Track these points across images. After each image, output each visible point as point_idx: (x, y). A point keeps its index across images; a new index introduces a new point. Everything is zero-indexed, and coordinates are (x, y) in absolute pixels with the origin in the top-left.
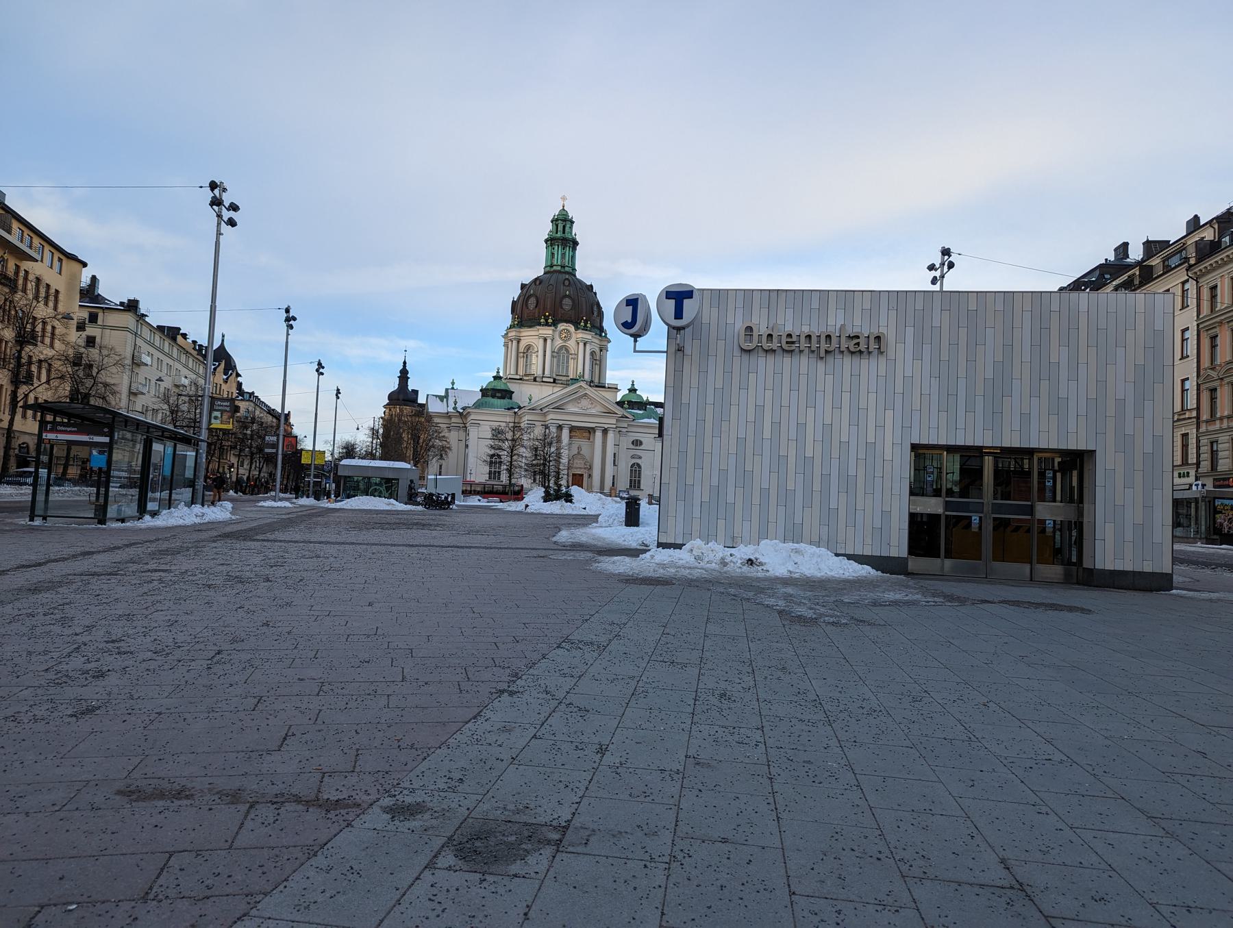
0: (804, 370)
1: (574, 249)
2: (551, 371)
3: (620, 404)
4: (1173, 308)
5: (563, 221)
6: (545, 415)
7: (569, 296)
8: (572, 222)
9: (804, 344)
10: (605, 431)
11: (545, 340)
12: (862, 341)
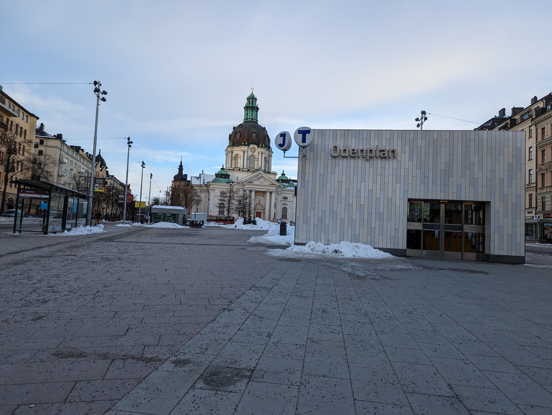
0: (360, 165)
1: (257, 111)
2: (247, 166)
3: (278, 181)
5: (252, 99)
6: (244, 185)
7: (255, 133)
8: (256, 99)
9: (360, 154)
10: (271, 193)
11: (244, 152)
12: (386, 152)
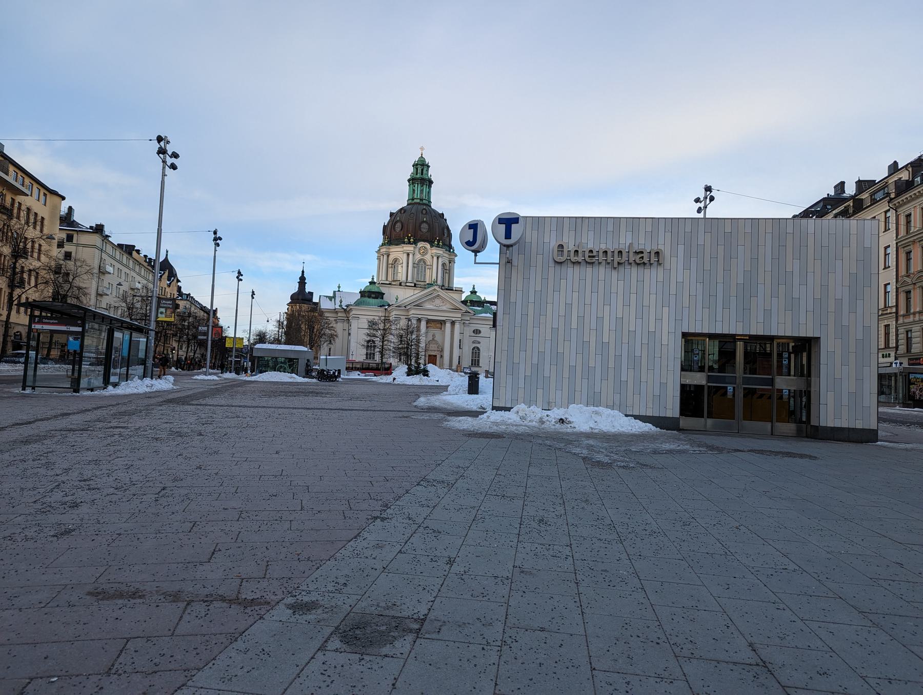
0: (602, 277)
1: (430, 187)
2: (413, 278)
3: (464, 302)
4: (878, 230)
5: (421, 166)
6: (408, 310)
7: (426, 222)
8: (428, 167)
9: (602, 258)
10: (453, 323)
11: (408, 255)
12: (645, 255)
